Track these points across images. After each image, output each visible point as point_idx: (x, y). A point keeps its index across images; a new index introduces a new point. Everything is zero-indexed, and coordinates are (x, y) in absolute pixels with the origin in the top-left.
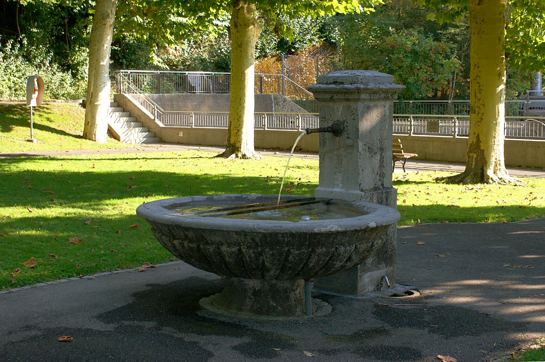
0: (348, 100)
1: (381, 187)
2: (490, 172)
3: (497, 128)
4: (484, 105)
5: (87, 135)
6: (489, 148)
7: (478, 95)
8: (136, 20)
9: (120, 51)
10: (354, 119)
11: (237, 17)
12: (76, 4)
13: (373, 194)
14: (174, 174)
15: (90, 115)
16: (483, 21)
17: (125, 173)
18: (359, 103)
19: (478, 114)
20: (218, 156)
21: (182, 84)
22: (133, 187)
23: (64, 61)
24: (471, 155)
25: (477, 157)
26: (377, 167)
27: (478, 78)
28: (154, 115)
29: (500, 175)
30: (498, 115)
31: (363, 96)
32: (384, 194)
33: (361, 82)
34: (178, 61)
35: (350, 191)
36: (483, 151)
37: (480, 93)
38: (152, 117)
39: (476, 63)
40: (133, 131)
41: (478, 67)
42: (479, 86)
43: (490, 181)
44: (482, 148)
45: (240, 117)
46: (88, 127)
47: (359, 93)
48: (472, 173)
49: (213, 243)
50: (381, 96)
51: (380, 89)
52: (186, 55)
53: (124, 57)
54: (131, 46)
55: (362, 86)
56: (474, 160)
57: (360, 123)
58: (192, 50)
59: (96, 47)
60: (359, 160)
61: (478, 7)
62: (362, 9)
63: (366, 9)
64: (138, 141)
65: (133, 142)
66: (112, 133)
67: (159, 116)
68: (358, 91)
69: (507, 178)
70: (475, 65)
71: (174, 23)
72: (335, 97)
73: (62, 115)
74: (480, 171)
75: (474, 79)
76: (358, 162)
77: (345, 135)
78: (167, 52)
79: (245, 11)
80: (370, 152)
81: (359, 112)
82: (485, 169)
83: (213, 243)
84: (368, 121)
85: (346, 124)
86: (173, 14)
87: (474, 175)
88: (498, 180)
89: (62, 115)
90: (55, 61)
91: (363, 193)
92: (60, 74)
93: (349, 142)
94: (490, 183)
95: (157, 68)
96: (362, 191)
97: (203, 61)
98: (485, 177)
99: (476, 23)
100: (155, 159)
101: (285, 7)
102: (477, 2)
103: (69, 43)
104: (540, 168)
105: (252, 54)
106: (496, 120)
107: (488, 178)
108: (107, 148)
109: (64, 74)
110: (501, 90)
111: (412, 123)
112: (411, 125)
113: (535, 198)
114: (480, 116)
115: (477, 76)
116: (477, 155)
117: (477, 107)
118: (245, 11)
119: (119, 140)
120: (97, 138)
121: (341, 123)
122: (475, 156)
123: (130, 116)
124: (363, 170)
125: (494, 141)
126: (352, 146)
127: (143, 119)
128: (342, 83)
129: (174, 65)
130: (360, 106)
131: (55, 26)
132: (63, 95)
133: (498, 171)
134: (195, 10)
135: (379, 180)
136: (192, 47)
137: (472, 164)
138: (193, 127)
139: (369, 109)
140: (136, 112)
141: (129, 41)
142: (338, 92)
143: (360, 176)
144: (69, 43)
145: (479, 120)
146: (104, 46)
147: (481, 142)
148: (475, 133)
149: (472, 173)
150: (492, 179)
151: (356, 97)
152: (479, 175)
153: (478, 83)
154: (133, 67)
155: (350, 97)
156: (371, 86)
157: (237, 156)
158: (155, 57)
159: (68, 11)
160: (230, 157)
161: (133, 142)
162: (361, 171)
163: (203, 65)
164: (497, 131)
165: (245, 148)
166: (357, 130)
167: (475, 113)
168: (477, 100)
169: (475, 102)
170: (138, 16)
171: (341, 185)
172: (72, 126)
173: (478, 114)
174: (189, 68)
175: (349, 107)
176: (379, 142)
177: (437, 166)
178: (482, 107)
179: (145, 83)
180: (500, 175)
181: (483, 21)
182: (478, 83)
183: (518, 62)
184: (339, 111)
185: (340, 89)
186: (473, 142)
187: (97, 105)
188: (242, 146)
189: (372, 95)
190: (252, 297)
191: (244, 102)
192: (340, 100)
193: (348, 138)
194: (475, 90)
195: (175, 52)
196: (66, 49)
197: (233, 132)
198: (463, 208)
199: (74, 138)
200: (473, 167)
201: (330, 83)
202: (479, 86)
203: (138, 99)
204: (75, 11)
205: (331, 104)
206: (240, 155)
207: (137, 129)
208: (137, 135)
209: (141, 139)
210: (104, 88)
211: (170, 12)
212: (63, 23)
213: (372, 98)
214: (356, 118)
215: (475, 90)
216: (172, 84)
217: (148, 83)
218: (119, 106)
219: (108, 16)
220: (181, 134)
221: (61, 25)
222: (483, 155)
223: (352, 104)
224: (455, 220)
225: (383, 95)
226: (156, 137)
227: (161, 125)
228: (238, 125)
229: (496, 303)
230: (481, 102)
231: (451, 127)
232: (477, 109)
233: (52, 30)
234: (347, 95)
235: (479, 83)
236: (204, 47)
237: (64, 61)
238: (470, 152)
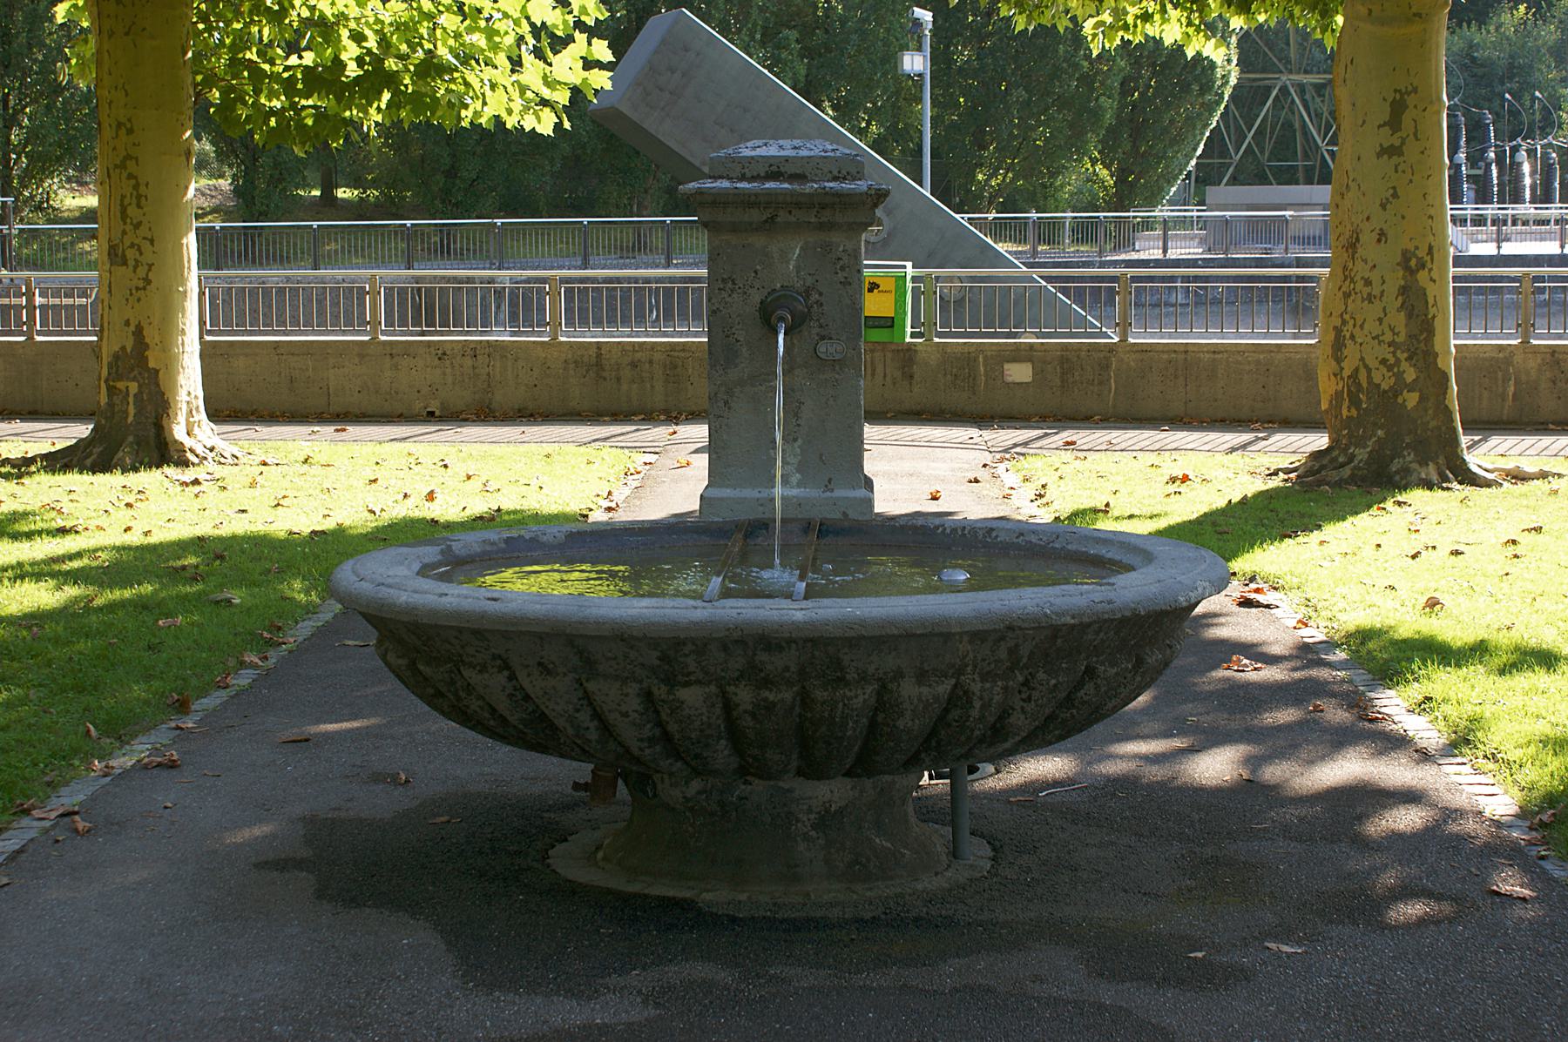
0: (821, 227)
2: (179, 432)
4: (152, 242)
6: (171, 363)
7: (132, 211)
19: (136, 267)
24: (121, 385)
25: (140, 392)
27: (131, 164)
36: (157, 372)
37: (139, 206)
39: (123, 120)
41: (130, 131)
42: (136, 187)
43: (190, 456)
44: (151, 364)
48: (131, 439)
49: (863, 678)
56: (131, 399)
70: (119, 125)
75: (116, 166)
82: (164, 423)
83: (863, 678)
85: (815, 297)
87: (138, 444)
107: (181, 449)
111: (38, 300)
112: (31, 307)
114: (141, 272)
115: (128, 157)
116: (140, 386)
117: (132, 245)
122: (134, 387)
128: (800, 177)
137: (126, 412)
142: (797, 203)
145: (141, 284)
147: (147, 347)
148: (127, 323)
149: (131, 439)
152: (152, 443)
153: (130, 176)
167: (125, 263)
168: (129, 228)
169: (124, 233)
173: (136, 267)
177: (18, 426)
178: (146, 246)
182: (130, 176)
184: (789, 260)
186: (123, 348)
190: (813, 833)
194: (123, 197)
200: (130, 419)
202: (136, 187)
205: (758, 241)
215: (123, 197)
229: (1177, 743)
230: (143, 231)
231: (19, 308)
232: (131, 254)
235: (136, 178)
238: (120, 378)
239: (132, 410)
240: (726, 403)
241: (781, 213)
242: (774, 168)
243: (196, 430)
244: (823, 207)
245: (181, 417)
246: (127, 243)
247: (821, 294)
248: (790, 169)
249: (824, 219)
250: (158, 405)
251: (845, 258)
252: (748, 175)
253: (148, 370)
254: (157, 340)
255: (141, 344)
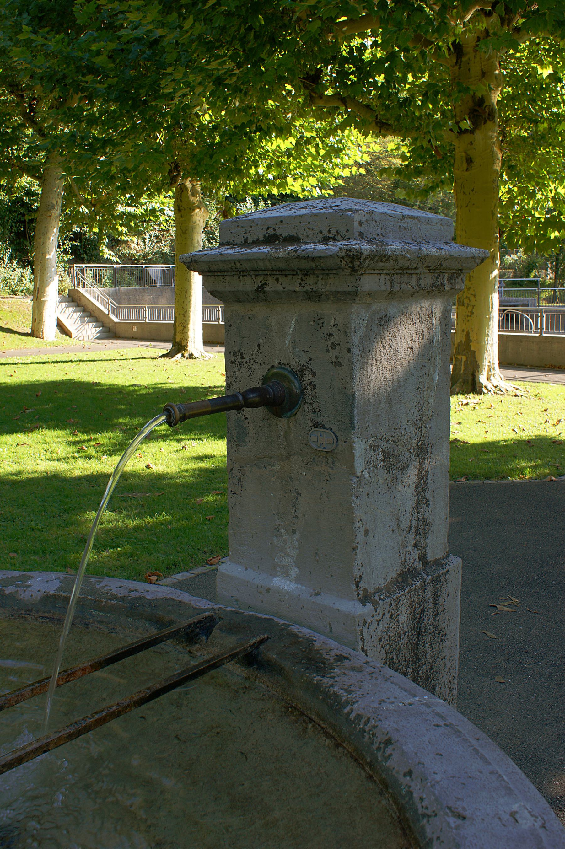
0: (314, 296)
1: (420, 566)
2: (483, 379)
3: (491, 323)
4: (475, 296)
5: (35, 333)
6: (481, 349)
8: (81, 210)
9: (81, 246)
10: (337, 364)
11: (181, 200)
12: (33, 200)
13: (398, 600)
14: (97, 384)
15: (36, 311)
16: (472, 190)
17: (28, 385)
18: (355, 308)
20: (163, 356)
21: (144, 278)
22: (27, 411)
23: (24, 258)
24: (459, 357)
25: (467, 360)
26: (409, 509)
28: (108, 309)
29: (495, 381)
30: (492, 308)
31: (369, 282)
32: (430, 588)
33: (361, 234)
34: (140, 255)
35: (327, 600)
36: (474, 352)
37: (470, 281)
38: (106, 312)
40: (86, 327)
43: (484, 390)
44: (472, 349)
45: (186, 312)
46: (36, 324)
47: (354, 270)
48: (461, 380)
50: (423, 283)
51: (423, 258)
52: (148, 249)
53: (86, 253)
54: (91, 241)
55: (366, 247)
56: (463, 363)
57: (357, 375)
58: (154, 244)
59: (42, 240)
60: (356, 502)
61: (466, 173)
62: (319, 191)
63: (323, 191)
64: (91, 337)
65: (86, 339)
66: (62, 328)
67: (114, 311)
68: (353, 262)
69: (504, 385)
71: (124, 214)
72: (272, 286)
73: (11, 312)
74: (470, 378)
76: (351, 509)
77: (304, 415)
78: (129, 247)
79: (190, 193)
80: (388, 468)
81: (356, 340)
82: (476, 374)
84: (385, 366)
85: (308, 377)
86: (122, 204)
87: (464, 383)
88: (493, 388)
89: (11, 312)
90: (16, 258)
91: (369, 606)
92: (19, 271)
93: (319, 439)
94: (484, 393)
95: (108, 261)
96: (365, 599)
97: (164, 255)
98: (477, 385)
99: (464, 193)
100: (90, 361)
101: (232, 183)
102: (465, 168)
103: (30, 239)
104: (522, 365)
105: (198, 241)
106: (489, 313)
107: (481, 385)
108: (54, 346)
109: (24, 271)
110: (495, 277)
113: (559, 421)
114: (470, 309)
117: (467, 297)
118: (190, 193)
119: (70, 337)
120: (44, 335)
121: (294, 374)
122: (464, 358)
123: (84, 311)
124: (366, 532)
125: (487, 340)
126: (329, 455)
127: (97, 314)
128: (294, 239)
129: (135, 260)
130: (359, 316)
131: (15, 223)
132: (22, 291)
133: (492, 377)
134: (125, 188)
135: (415, 546)
136: (153, 242)
137: (460, 369)
138: (147, 321)
139: (384, 322)
140: (90, 307)
141: (90, 236)
142: (281, 270)
143: (360, 557)
144: (30, 239)
145: (469, 314)
146: (49, 239)
147: (471, 341)
148: (463, 331)
149: (461, 380)
150: (486, 387)
151: (341, 284)
154: (94, 262)
155: (321, 286)
156: (394, 246)
157: (183, 356)
158: (106, 250)
159: (28, 207)
160: (175, 358)
161: (86, 339)
162: (360, 538)
163: (163, 258)
164: (491, 327)
165: (193, 347)
166: (348, 399)
167: (463, 305)
170: (83, 206)
171: (294, 572)
172: (20, 323)
174: (150, 262)
175: (319, 321)
176: (413, 430)
178: (472, 298)
179: (106, 278)
180: (495, 381)
181: (472, 190)
183: (518, 241)
184: (286, 332)
185: (287, 260)
186: (461, 341)
187: (44, 301)
188: (189, 344)
189: (396, 278)
191: (190, 295)
192: (289, 296)
193: (316, 425)
195: (137, 247)
196: (26, 246)
197: (179, 329)
198: (474, 445)
199: (20, 337)
200: (462, 372)
201: (256, 243)
203: (93, 294)
204: (34, 207)
205: (259, 311)
206: (186, 355)
207: (91, 324)
208: (91, 330)
209: (95, 334)
210: (52, 283)
211: (118, 202)
212: (22, 219)
213: (396, 288)
214: (345, 356)
216: (133, 278)
217: (108, 278)
218: (73, 301)
219: (53, 207)
220: (135, 329)
221: (20, 221)
222: (475, 358)
223: (327, 309)
224: (476, 477)
225: (428, 280)
226: (111, 332)
227: (116, 320)
228: (184, 321)
230: (471, 291)
232: (466, 301)
233: (12, 227)
234: (311, 280)
236: (165, 241)
237: (24, 258)
238: (458, 353)
239: (463, 368)
240: (239, 480)
241: (271, 281)
242: (271, 232)
243: (492, 378)
244: (306, 273)
245: (485, 373)
246: (465, 296)
247: (314, 374)
248: (284, 232)
249: (308, 288)
250: (474, 367)
251: (336, 333)
252: (250, 241)
253: (471, 351)
254: (475, 338)
255: (468, 340)
